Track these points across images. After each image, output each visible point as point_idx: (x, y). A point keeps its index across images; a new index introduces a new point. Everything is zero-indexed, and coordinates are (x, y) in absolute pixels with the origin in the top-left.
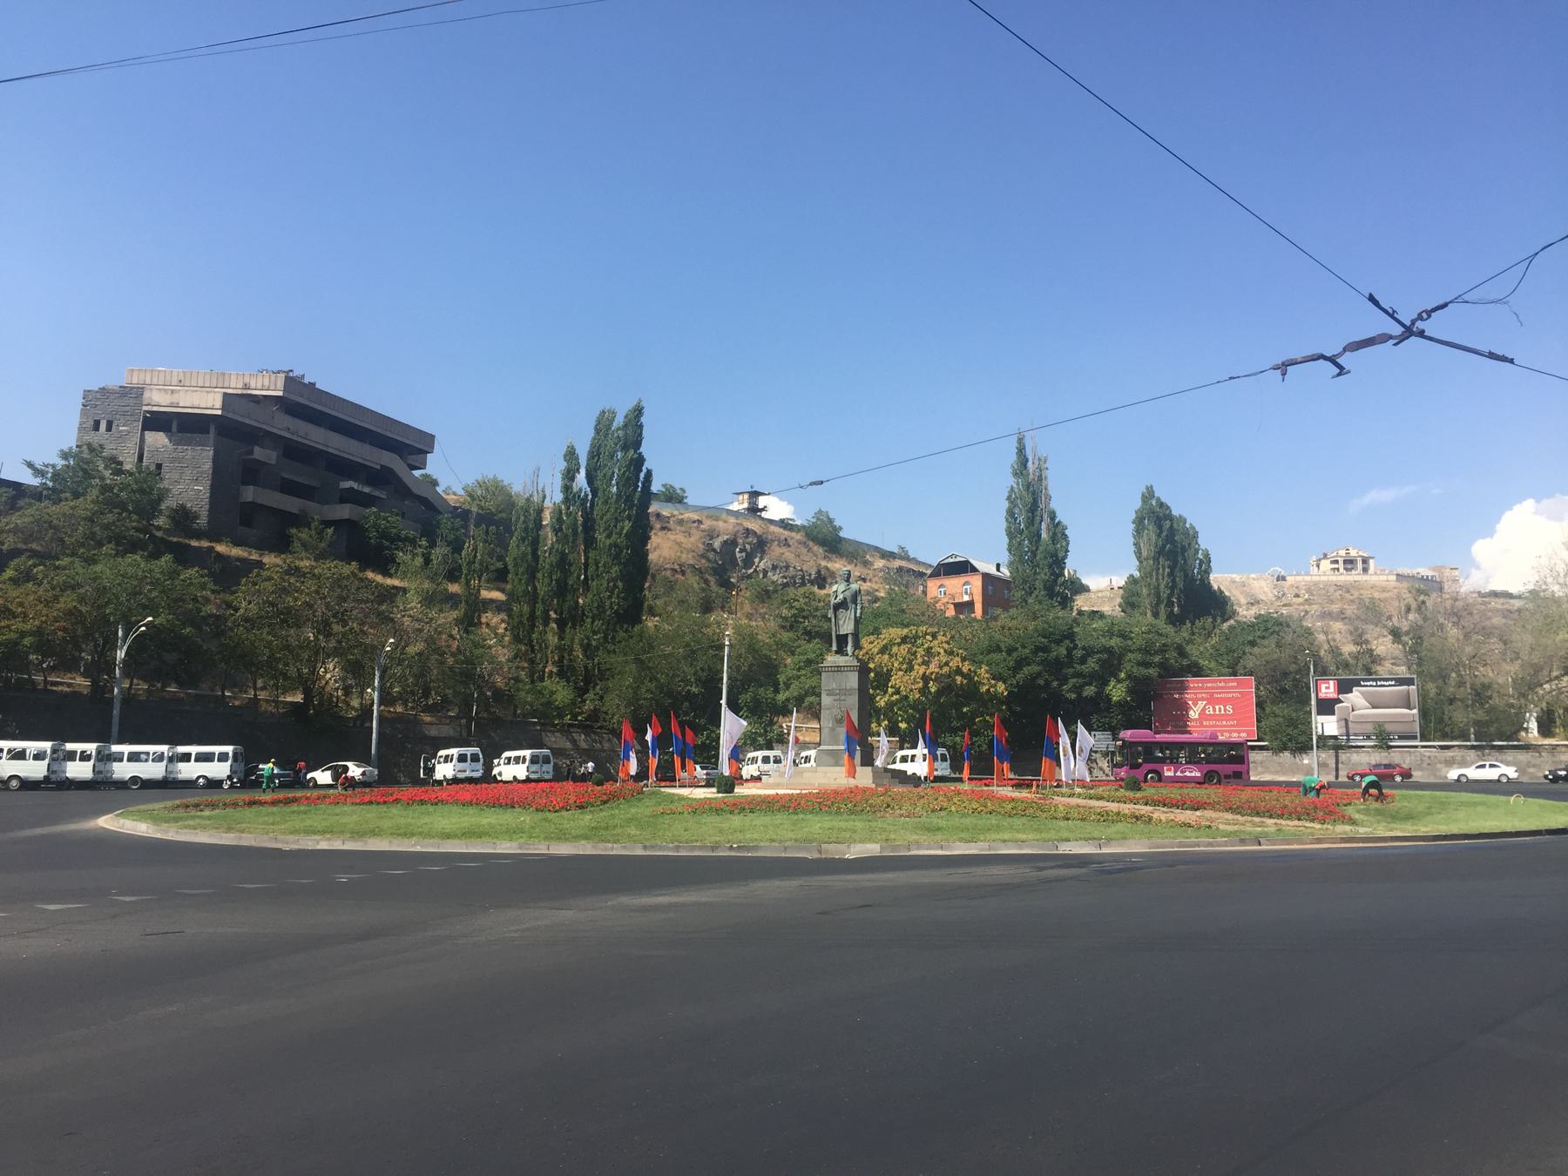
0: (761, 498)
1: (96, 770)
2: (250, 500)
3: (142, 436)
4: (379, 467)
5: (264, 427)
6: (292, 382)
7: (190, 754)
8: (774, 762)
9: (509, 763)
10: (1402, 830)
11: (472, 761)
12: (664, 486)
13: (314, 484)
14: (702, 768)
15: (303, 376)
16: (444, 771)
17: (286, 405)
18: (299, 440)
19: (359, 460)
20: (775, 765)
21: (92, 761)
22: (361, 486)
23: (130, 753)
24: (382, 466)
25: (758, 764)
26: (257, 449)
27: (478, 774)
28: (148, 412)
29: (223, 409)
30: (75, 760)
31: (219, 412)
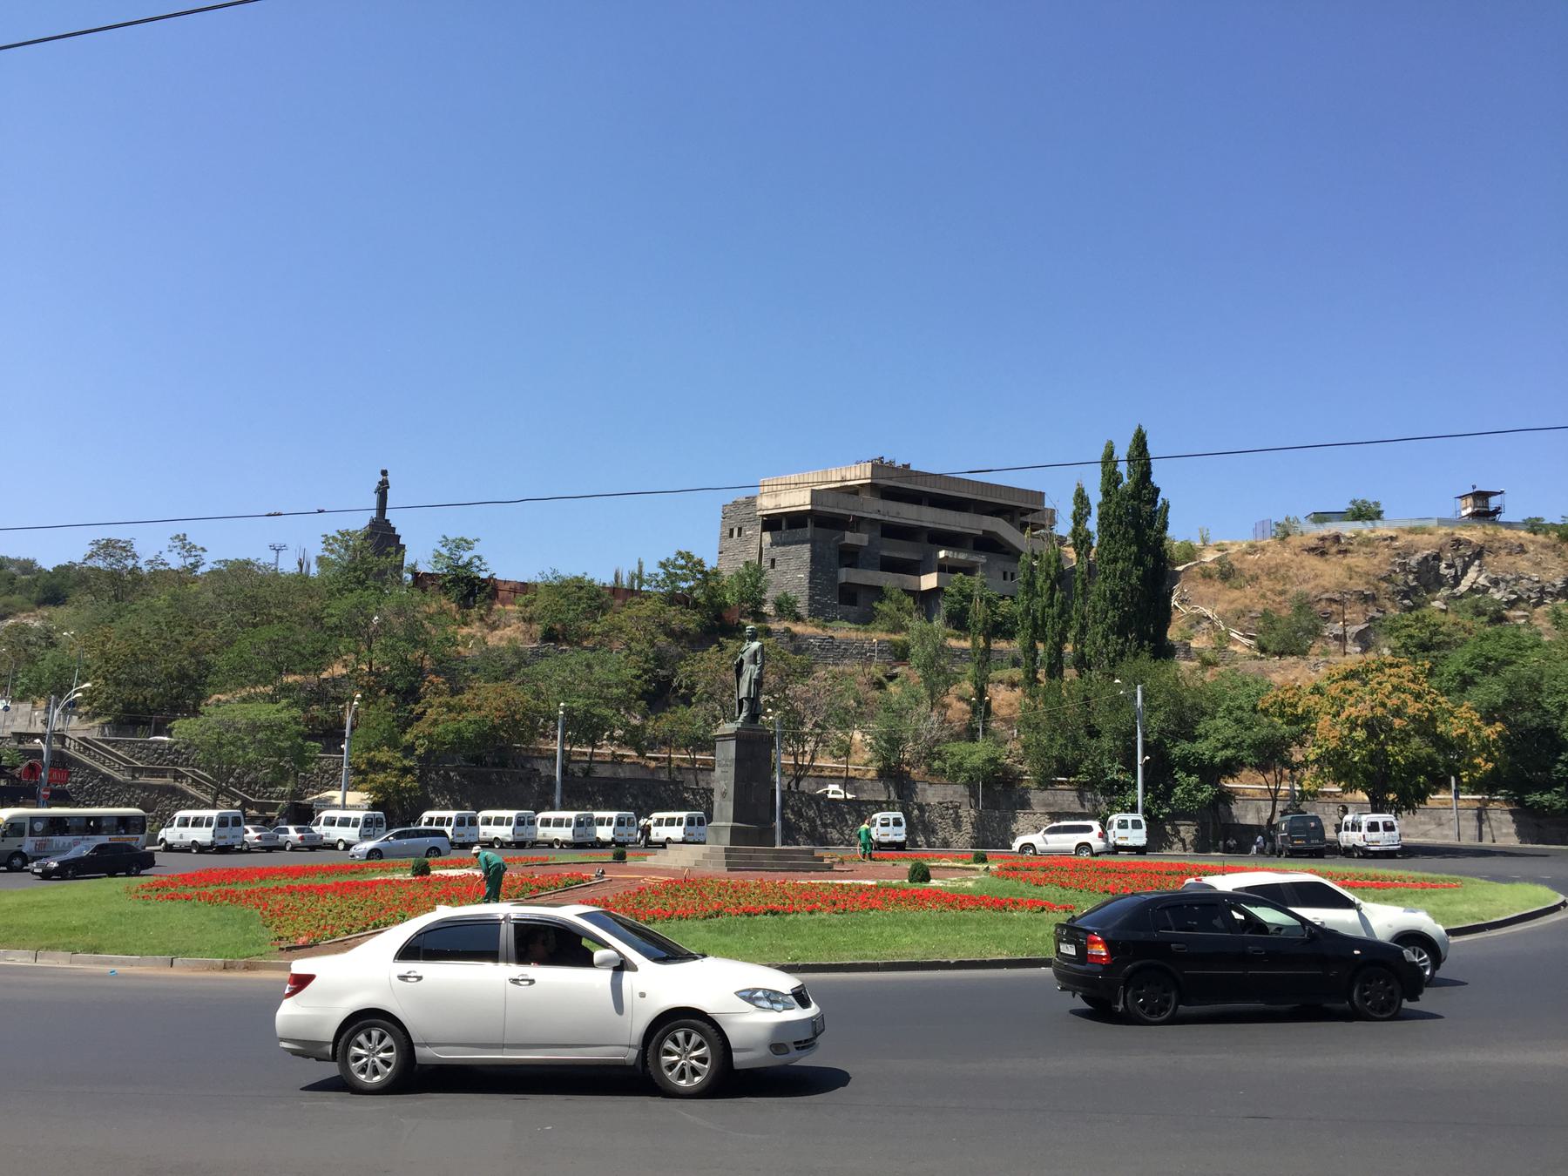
1: (687, 833)
2: (844, 581)
3: (761, 535)
4: (981, 533)
6: (879, 466)
8: (894, 825)
9: (186, 825)
10: (1000, 941)
11: (894, 825)
12: (1354, 502)
13: (915, 557)
14: (298, 831)
17: (875, 489)
18: (891, 519)
19: (958, 529)
20: (1387, 833)
21: (683, 826)
22: (955, 554)
25: (1114, 830)
26: (848, 534)
27: (902, 838)
28: (763, 516)
29: (811, 504)
30: (349, 826)
31: (809, 507)
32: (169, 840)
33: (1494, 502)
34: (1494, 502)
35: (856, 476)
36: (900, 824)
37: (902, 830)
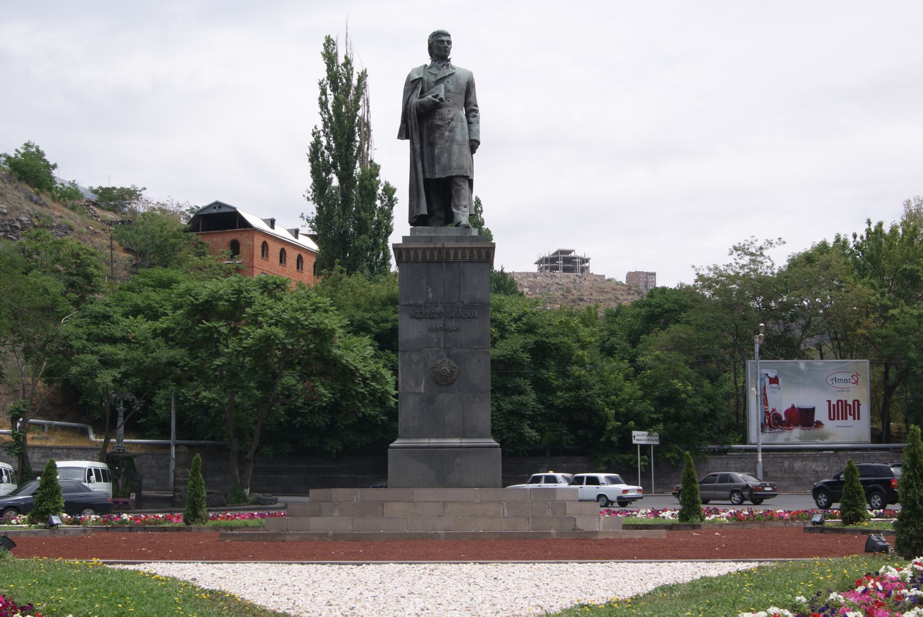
15: (55, 166)
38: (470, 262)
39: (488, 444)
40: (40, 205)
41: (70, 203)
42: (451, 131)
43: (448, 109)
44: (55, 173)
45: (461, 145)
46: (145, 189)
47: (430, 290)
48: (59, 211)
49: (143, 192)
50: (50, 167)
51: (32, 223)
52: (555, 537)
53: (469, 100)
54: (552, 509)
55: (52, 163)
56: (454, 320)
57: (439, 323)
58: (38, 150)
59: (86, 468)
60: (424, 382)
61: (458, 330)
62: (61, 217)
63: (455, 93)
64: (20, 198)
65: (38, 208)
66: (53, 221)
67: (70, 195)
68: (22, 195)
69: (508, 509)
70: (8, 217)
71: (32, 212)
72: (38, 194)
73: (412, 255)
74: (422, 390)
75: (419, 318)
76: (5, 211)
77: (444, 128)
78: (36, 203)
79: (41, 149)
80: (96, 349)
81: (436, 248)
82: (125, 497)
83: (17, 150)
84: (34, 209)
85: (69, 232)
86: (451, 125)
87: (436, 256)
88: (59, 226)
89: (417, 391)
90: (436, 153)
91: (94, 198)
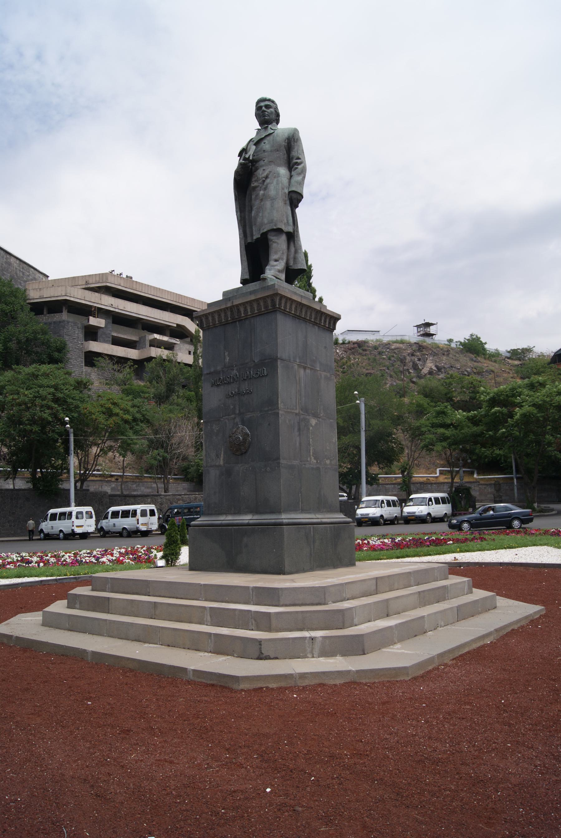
0: (431, 327)
4: (175, 325)
5: (95, 305)
7: (118, 512)
15: (486, 343)
16: (365, 549)
23: (56, 520)
24: (177, 325)
26: (91, 318)
30: (118, 518)
32: (46, 531)
33: (432, 330)
34: (432, 330)
35: (96, 281)
36: (91, 517)
37: (155, 519)
38: (260, 314)
39: (273, 521)
40: (477, 362)
41: (493, 359)
42: (265, 189)
43: (262, 169)
44: (486, 346)
45: (274, 199)
46: (534, 347)
47: (226, 354)
48: (487, 364)
49: (534, 349)
50: (482, 344)
51: (473, 371)
52: (192, 678)
53: (291, 155)
54: (255, 621)
55: (484, 342)
56: (246, 382)
57: (233, 388)
58: (477, 336)
59: (427, 498)
60: (222, 453)
61: (249, 393)
62: (488, 366)
63: (271, 151)
64: (466, 360)
65: (476, 364)
66: (483, 369)
67: (495, 356)
68: (468, 359)
69: (211, 617)
70: (461, 370)
71: (472, 366)
72: (476, 357)
73: (211, 321)
74: (222, 463)
75: (218, 385)
76: (459, 367)
77: (259, 188)
78: (475, 361)
79: (478, 336)
80: (435, 431)
81: (227, 308)
82: (466, 511)
83: (465, 338)
84: (474, 365)
85: (492, 373)
86: (265, 184)
87: (229, 316)
88: (486, 371)
89: (217, 464)
90: (253, 215)
91: (508, 355)
